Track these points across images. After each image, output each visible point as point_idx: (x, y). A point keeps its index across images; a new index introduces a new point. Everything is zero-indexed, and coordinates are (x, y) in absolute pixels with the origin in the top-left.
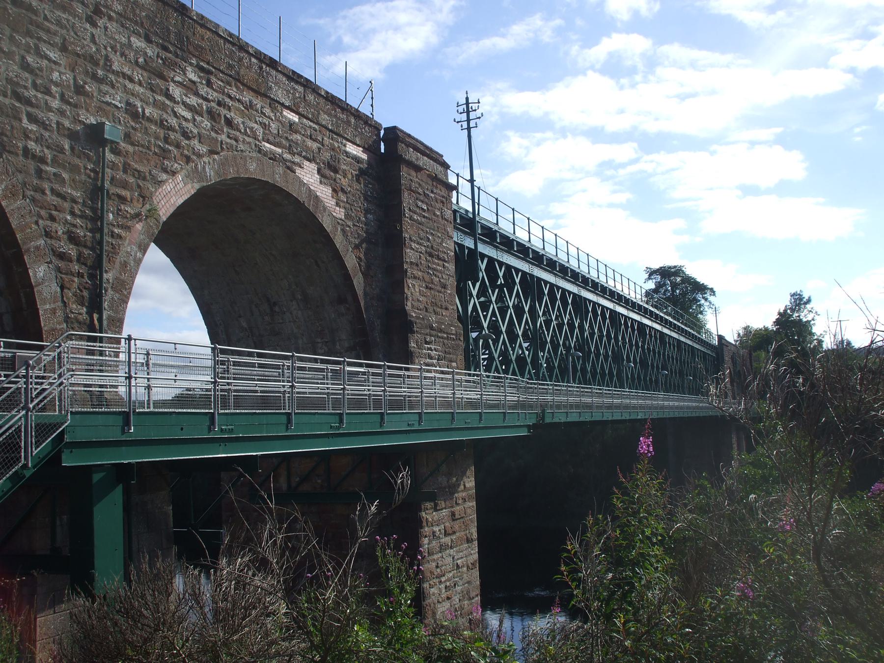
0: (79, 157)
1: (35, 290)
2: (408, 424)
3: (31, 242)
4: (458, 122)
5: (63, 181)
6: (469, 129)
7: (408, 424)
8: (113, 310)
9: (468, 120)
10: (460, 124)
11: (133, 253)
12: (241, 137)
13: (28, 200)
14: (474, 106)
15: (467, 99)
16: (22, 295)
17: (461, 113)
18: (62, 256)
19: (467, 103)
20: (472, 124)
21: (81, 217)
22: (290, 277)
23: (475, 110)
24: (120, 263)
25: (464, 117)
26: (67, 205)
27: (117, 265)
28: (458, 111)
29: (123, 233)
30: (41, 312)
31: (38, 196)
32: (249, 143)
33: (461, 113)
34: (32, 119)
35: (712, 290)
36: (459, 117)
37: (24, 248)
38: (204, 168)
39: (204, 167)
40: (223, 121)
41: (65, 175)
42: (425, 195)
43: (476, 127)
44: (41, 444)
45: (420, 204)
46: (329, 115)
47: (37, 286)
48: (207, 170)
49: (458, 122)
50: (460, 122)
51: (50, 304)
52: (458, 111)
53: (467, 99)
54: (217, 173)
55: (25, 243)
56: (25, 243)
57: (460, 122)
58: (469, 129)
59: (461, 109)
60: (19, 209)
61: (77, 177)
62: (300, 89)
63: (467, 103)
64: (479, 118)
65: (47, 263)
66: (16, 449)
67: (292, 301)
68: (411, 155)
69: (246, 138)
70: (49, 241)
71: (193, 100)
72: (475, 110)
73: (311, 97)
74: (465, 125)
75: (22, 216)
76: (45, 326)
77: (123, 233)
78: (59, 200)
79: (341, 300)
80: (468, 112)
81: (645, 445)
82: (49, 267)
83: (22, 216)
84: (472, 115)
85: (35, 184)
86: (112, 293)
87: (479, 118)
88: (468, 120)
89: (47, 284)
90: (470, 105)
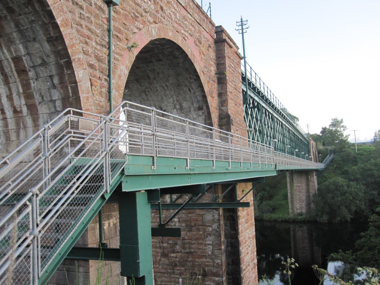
0: (99, 10)
1: (78, 84)
2: (226, 169)
3: (76, 55)
4: (237, 30)
5: (91, 22)
6: (243, 33)
7: (226, 169)
8: (115, 101)
9: (242, 29)
10: (238, 31)
11: (123, 71)
12: (166, 18)
13: (74, 30)
14: (245, 23)
15: (242, 19)
16: (69, 88)
17: (239, 26)
18: (91, 66)
19: (242, 21)
20: (244, 31)
21: (100, 45)
22: (174, 97)
23: (246, 25)
24: (118, 75)
25: (240, 28)
26: (93, 36)
27: (117, 77)
28: (237, 25)
29: (120, 58)
30: (81, 98)
31: (79, 28)
32: (169, 21)
33: (239, 26)
35: (297, 118)
36: (237, 28)
37: (72, 58)
38: (152, 30)
39: (152, 29)
40: (159, 7)
41: (92, 19)
42: (233, 60)
43: (246, 32)
44: (114, 176)
45: (231, 64)
46: (198, 15)
47: (79, 82)
48: (153, 31)
49: (237, 30)
50: (238, 30)
51: (86, 94)
52: (237, 25)
53: (242, 19)
54: (157, 34)
55: (73, 56)
56: (73, 56)
57: (238, 30)
58: (243, 33)
59: (238, 24)
60: (69, 34)
61: (98, 22)
63: (242, 21)
64: (248, 28)
65: (83, 69)
66: (101, 180)
67: (174, 109)
69: (168, 18)
70: (85, 56)
72: (246, 25)
74: (241, 31)
75: (71, 39)
76: (83, 107)
77: (120, 58)
78: (89, 32)
79: (200, 109)
80: (242, 25)
81: (217, 195)
82: (85, 72)
83: (71, 39)
84: (244, 27)
85: (77, 21)
86: (115, 91)
87: (248, 28)
88: (242, 29)
89: (84, 82)
90: (243, 22)
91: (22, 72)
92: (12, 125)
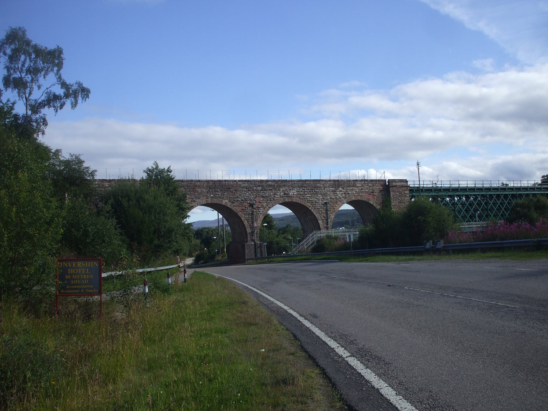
15: (418, 162)
19: (418, 163)
34: (318, 204)
53: (418, 162)
62: (363, 182)
63: (418, 163)
68: (394, 184)
71: (341, 193)
73: (366, 182)
91: (312, 221)
92: (312, 230)
